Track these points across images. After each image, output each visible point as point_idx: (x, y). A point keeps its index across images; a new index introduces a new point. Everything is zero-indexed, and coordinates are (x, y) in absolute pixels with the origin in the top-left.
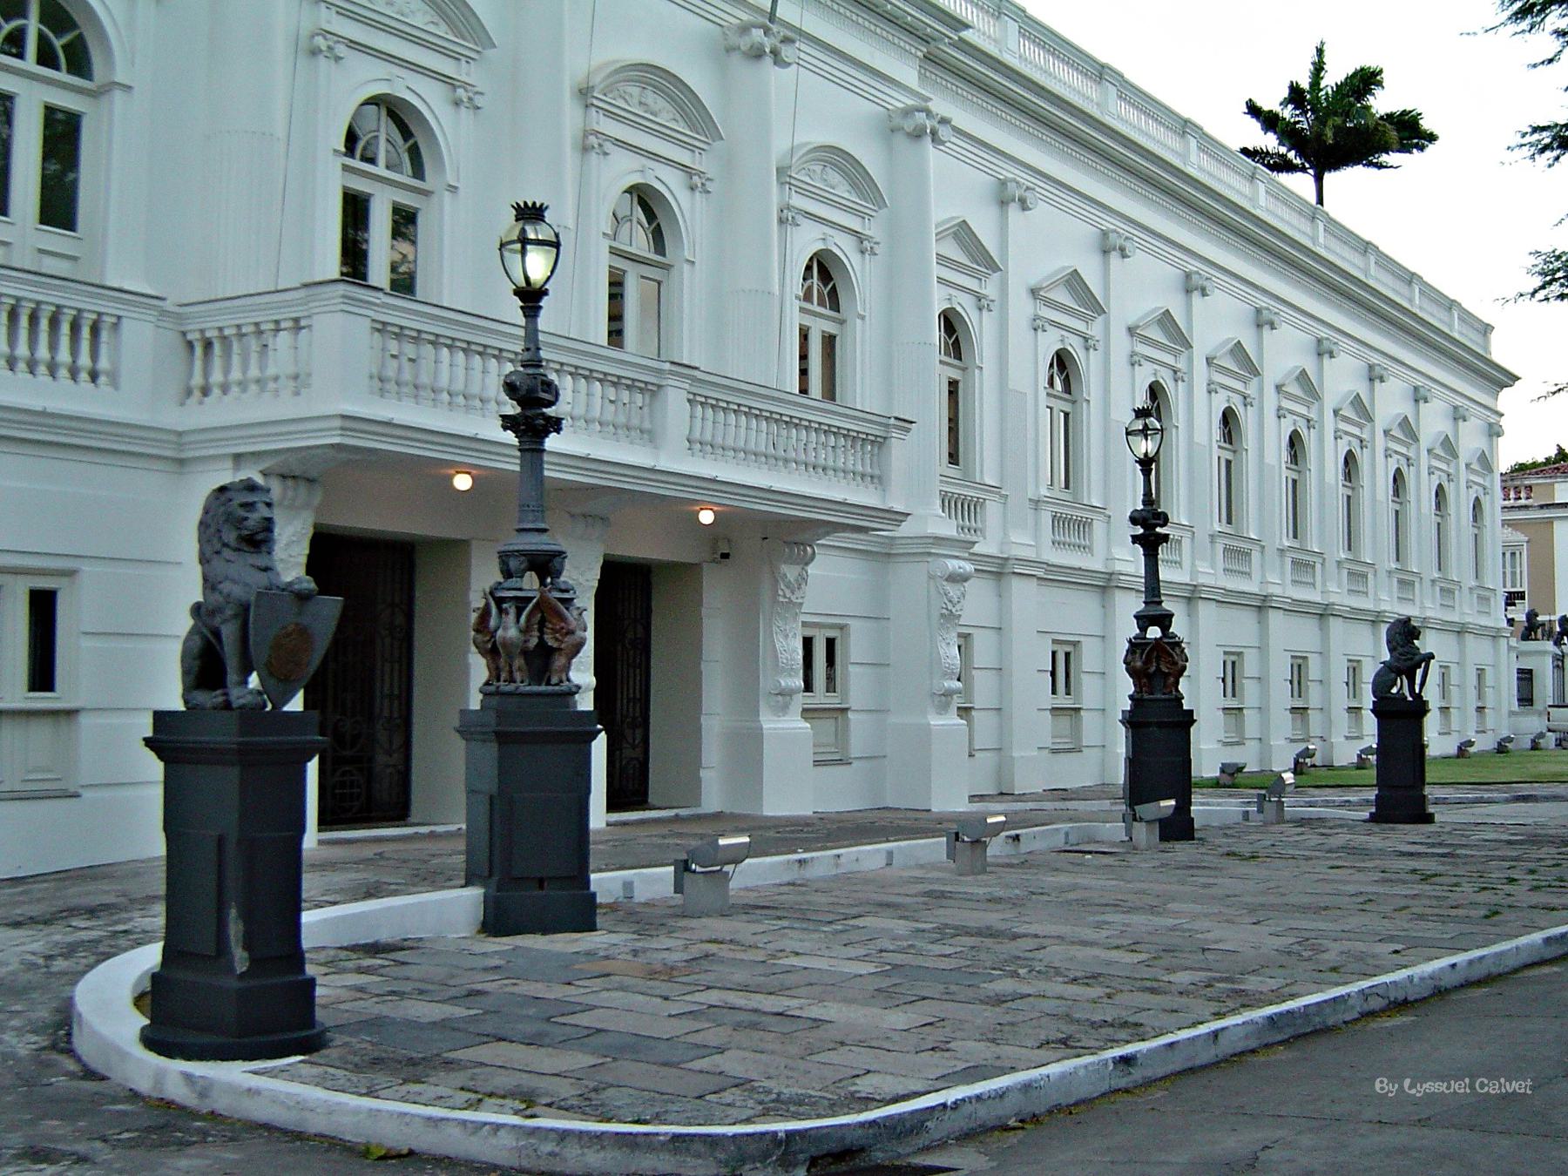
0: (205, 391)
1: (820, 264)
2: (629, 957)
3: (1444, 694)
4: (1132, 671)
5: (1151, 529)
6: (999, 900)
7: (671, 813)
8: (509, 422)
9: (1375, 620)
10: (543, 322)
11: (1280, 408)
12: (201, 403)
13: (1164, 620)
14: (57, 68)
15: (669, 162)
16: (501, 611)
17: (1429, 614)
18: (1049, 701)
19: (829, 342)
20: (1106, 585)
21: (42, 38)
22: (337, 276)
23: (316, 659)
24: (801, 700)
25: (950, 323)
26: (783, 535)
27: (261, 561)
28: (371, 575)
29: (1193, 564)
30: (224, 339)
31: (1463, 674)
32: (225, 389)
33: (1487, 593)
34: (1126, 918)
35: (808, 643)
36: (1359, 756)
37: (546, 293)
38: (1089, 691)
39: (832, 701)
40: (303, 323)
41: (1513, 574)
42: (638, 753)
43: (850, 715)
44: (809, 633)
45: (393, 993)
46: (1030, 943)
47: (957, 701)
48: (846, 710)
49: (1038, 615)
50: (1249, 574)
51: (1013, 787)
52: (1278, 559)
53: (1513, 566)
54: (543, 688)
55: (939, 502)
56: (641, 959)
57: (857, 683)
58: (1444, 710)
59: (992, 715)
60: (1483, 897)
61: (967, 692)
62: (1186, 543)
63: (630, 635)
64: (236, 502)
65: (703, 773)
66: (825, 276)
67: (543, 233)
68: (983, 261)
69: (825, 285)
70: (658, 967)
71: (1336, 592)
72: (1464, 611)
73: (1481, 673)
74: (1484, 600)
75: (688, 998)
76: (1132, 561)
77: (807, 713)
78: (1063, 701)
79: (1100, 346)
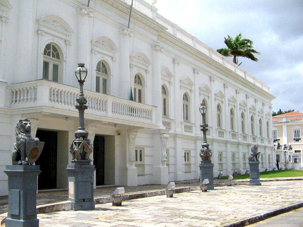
0: (16, 101)
1: (103, 63)
2: (102, 215)
3: (262, 160)
4: (201, 156)
5: (205, 129)
6: (176, 202)
7: (109, 186)
8: (77, 107)
9: (249, 145)
10: (84, 87)
11: (229, 104)
12: (15, 104)
13: (207, 146)
14: (55, 58)
15: (108, 55)
16: (75, 145)
17: (259, 144)
18: (184, 162)
19: (105, 81)
20: (196, 139)
21: (52, 52)
22: (42, 78)
23: (39, 154)
24: (135, 163)
25: (164, 88)
26: (132, 129)
27: (28, 135)
28: (50, 138)
29: (212, 135)
30: (20, 91)
31: (265, 156)
32: (20, 101)
33: (255, 137)
34: (202, 206)
35: (136, 151)
36: (246, 173)
37: (84, 81)
38: (192, 160)
39: (141, 163)
40: (35, 88)
41: (275, 136)
42: (102, 174)
43: (191, 165)
44: (136, 149)
45: (54, 222)
46: (183, 211)
47: (166, 163)
48: (144, 164)
49: (181, 146)
50: (256, 141)
51: (127, 183)
52: (229, 134)
53: (275, 134)
54: (84, 161)
55: (162, 123)
56: (104, 215)
57: (147, 160)
58: (262, 163)
59: (225, 164)
60: (272, 200)
61: (168, 161)
62: (211, 130)
63: (100, 150)
64: (23, 123)
65: (115, 178)
66: (139, 78)
67: (84, 69)
68: (169, 75)
69: (104, 68)
70: (108, 216)
71: (241, 140)
72: (266, 143)
73: (269, 156)
74: (269, 141)
75: (114, 223)
76: (201, 134)
77: (136, 165)
78: (220, 162)
79: (224, 103)
